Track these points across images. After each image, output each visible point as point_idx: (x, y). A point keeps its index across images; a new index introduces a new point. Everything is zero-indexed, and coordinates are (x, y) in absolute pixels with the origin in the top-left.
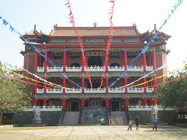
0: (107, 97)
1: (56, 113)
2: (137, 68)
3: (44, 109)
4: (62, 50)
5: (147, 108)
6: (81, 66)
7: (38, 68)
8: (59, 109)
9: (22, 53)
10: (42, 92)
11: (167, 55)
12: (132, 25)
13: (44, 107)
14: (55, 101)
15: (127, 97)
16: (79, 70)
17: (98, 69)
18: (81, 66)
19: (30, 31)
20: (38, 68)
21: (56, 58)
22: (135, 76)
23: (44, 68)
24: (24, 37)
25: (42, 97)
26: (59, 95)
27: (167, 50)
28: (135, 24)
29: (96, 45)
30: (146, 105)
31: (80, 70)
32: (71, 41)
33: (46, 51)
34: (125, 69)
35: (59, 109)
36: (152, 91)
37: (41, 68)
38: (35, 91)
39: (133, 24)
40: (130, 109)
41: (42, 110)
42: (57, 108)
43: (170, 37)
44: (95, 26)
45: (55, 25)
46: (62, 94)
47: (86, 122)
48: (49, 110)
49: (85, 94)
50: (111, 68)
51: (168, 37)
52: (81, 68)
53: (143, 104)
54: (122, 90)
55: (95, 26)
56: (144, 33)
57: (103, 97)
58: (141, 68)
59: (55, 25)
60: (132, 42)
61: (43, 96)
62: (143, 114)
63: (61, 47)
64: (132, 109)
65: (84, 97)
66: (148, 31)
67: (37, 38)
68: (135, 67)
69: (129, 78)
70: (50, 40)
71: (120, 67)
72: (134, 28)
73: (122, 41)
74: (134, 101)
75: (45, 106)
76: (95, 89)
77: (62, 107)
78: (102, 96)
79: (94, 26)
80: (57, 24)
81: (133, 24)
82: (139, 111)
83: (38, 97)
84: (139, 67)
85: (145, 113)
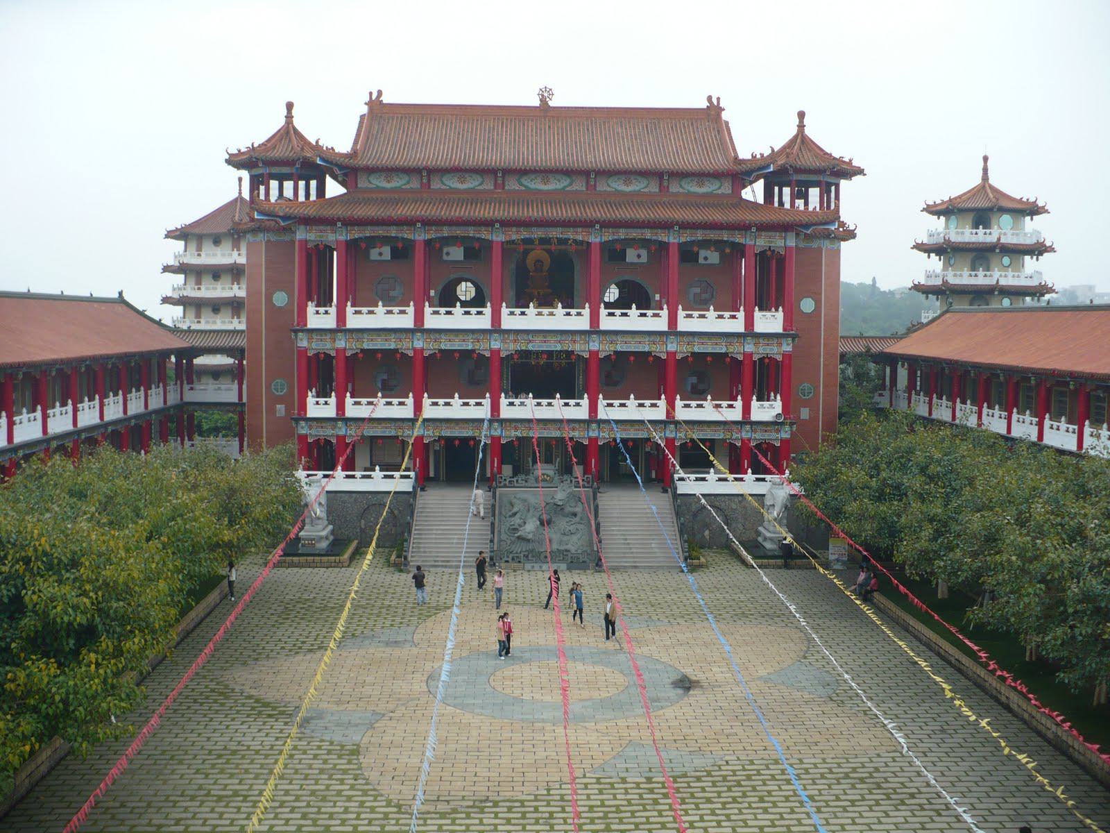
0: (593, 434)
2: (720, 317)
3: (340, 481)
4: (580, 235)
5: (749, 485)
6: (489, 304)
8: (400, 483)
12: (704, 104)
13: (339, 473)
14: (382, 448)
15: (672, 435)
17: (559, 319)
18: (489, 304)
19: (259, 130)
20: (311, 308)
22: (710, 350)
23: (333, 310)
25: (329, 432)
26: (438, 424)
28: (718, 99)
30: (746, 473)
32: (609, 185)
33: (343, 238)
35: (400, 483)
38: (303, 407)
39: (710, 99)
40: (682, 488)
41: (332, 486)
42: (391, 477)
43: (860, 172)
45: (371, 94)
46: (413, 421)
47: (511, 556)
48: (358, 485)
49: (677, 423)
52: (488, 310)
53: (736, 468)
54: (522, 407)
57: (576, 434)
58: (734, 317)
59: (374, 97)
60: (389, 186)
61: (334, 428)
62: (734, 506)
64: (689, 485)
65: (342, 432)
68: (380, 309)
69: (507, 356)
70: (356, 179)
71: (650, 312)
72: (710, 117)
74: (696, 459)
75: (343, 470)
76: (544, 402)
77: (412, 474)
78: (573, 429)
80: (380, 93)
81: (710, 99)
83: (313, 432)
84: (727, 314)
85: (740, 502)
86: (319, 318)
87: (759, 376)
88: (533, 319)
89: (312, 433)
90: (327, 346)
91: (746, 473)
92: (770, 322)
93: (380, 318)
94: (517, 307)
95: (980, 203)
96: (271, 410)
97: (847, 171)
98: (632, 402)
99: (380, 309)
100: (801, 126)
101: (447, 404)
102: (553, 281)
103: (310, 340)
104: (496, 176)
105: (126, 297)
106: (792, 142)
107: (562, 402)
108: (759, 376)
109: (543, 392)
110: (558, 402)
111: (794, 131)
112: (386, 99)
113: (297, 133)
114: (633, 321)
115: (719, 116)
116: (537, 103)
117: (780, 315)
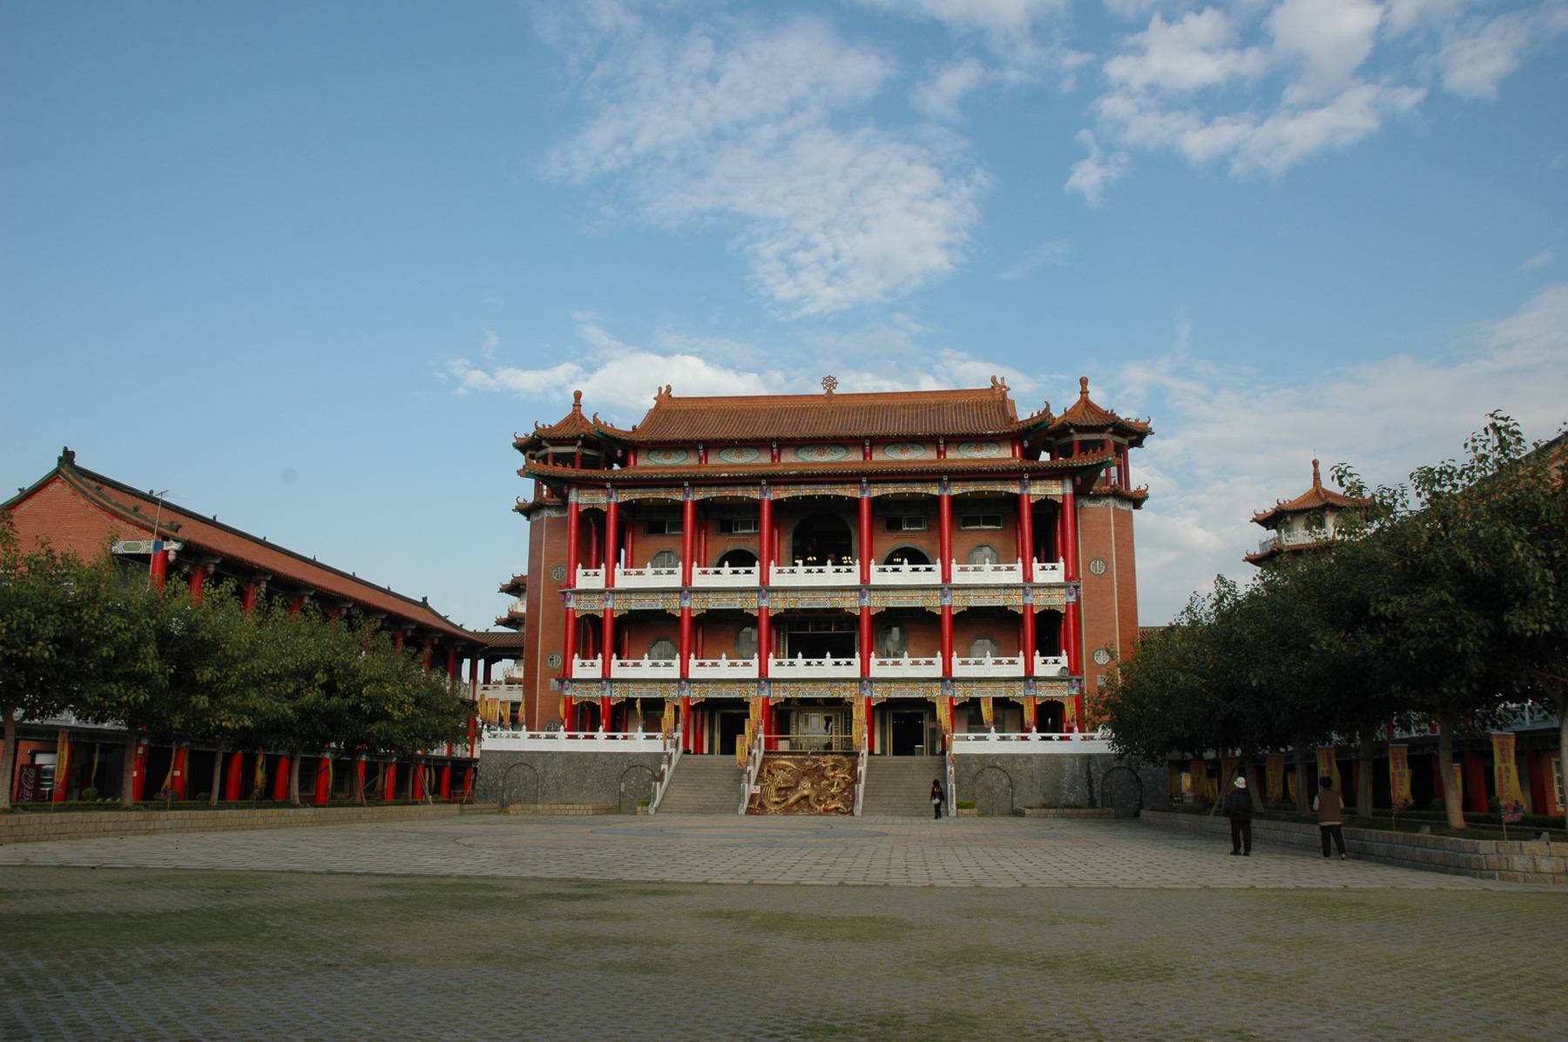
1: (647, 762)
4: (848, 492)
7: (580, 571)
9: (527, 511)
10: (596, 673)
11: (1136, 512)
12: (989, 385)
13: (601, 734)
16: (749, 578)
17: (829, 576)
20: (580, 571)
21: (646, 524)
24: (529, 446)
27: (1133, 488)
29: (116, 505)
31: (752, 580)
34: (944, 580)
36: (1058, 667)
37: (1048, 566)
39: (994, 379)
42: (1050, 739)
44: (830, 391)
48: (620, 745)
49: (770, 681)
50: (962, 570)
51: (1135, 435)
55: (830, 391)
56: (1032, 418)
63: (674, 483)
66: (1047, 410)
67: (584, 446)
68: (649, 570)
73: (773, 458)
79: (824, 392)
80: (669, 388)
81: (994, 379)
82: (998, 756)
86: (589, 579)
87: (1048, 631)
88: (801, 576)
89: (576, 693)
90: (596, 606)
91: (988, 731)
92: (1050, 574)
93: (649, 578)
94: (1047, 561)
95: (1316, 503)
96: (545, 684)
97: (1135, 435)
98: (724, 662)
99: (649, 570)
100: (1084, 392)
101: (714, 665)
102: (821, 531)
103: (577, 601)
104: (863, 446)
105: (430, 603)
106: (566, 422)
107: (728, 662)
108: (1048, 631)
109: (814, 651)
110: (828, 660)
111: (1078, 397)
112: (674, 394)
113: (582, 417)
114: (906, 575)
115: (1004, 395)
116: (820, 390)
117: (1061, 565)
